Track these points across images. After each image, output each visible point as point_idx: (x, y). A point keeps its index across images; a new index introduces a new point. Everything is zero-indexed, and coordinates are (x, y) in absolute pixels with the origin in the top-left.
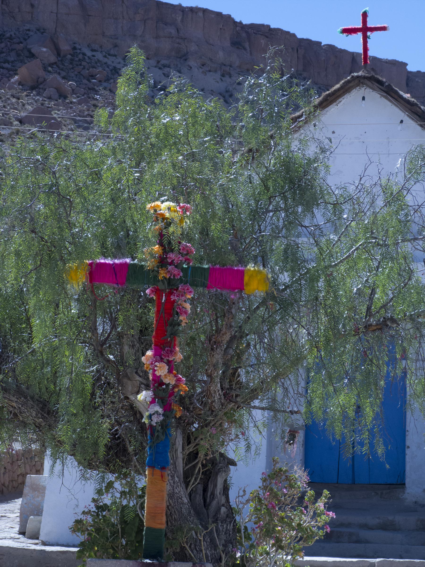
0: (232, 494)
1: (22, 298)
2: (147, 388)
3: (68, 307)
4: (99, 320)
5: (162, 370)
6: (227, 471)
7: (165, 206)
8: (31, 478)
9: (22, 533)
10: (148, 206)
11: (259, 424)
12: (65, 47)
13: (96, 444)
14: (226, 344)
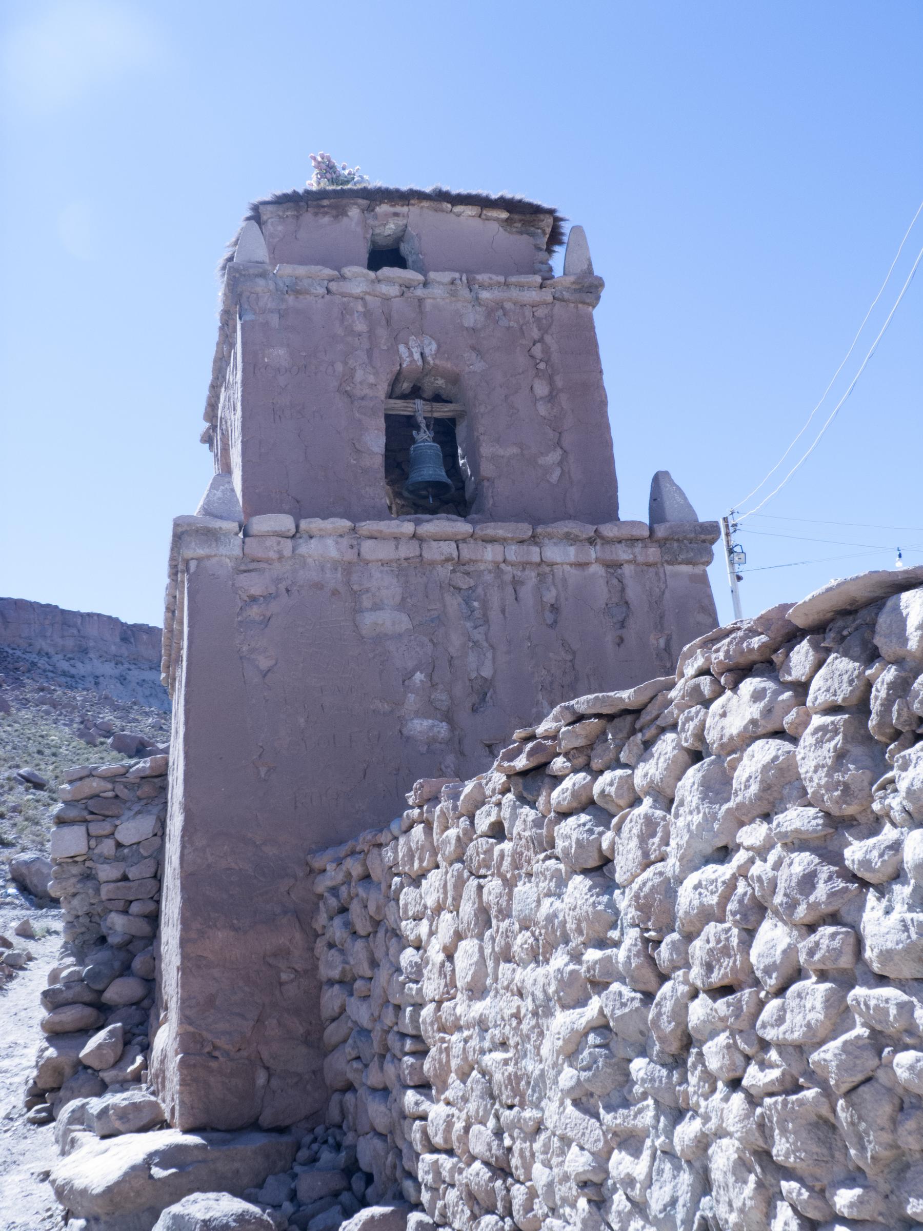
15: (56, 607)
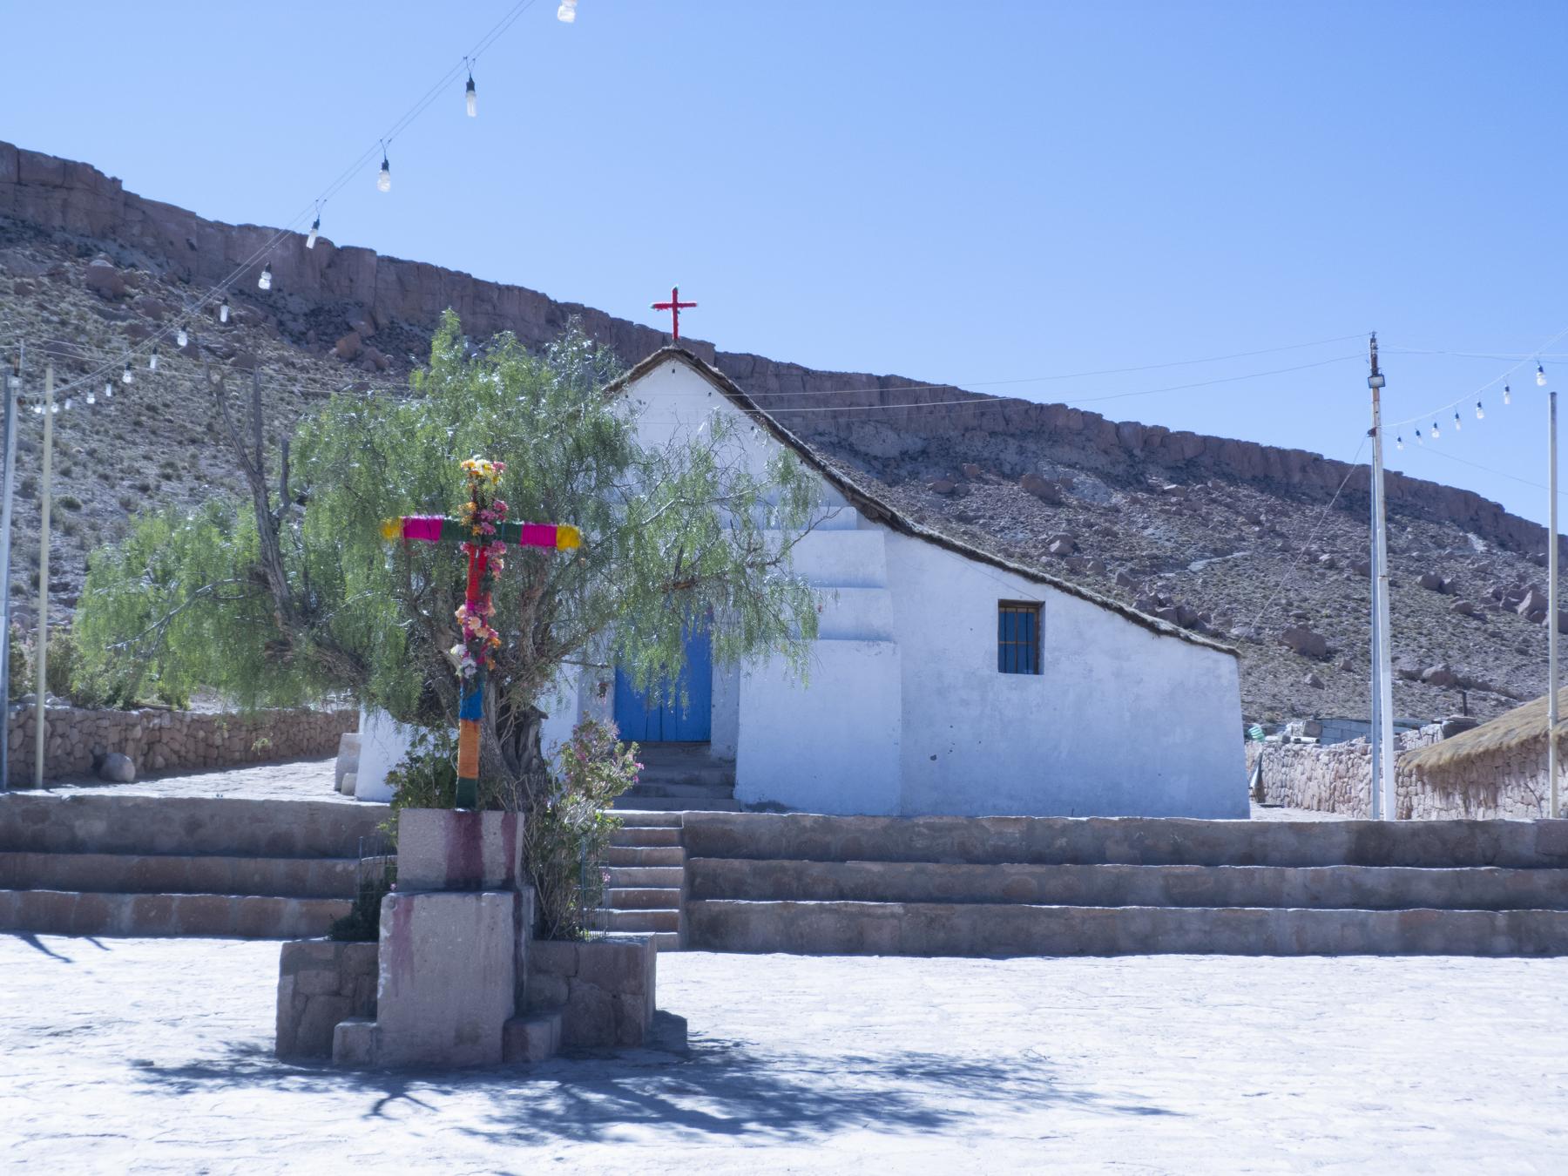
0: (544, 745)
1: (336, 554)
2: (461, 642)
3: (382, 562)
4: (413, 576)
5: (475, 624)
6: (539, 724)
7: (479, 463)
8: (347, 736)
9: (338, 789)
10: (462, 464)
11: (571, 679)
12: (383, 321)
13: (409, 697)
14: (538, 597)
15: (469, 276)
